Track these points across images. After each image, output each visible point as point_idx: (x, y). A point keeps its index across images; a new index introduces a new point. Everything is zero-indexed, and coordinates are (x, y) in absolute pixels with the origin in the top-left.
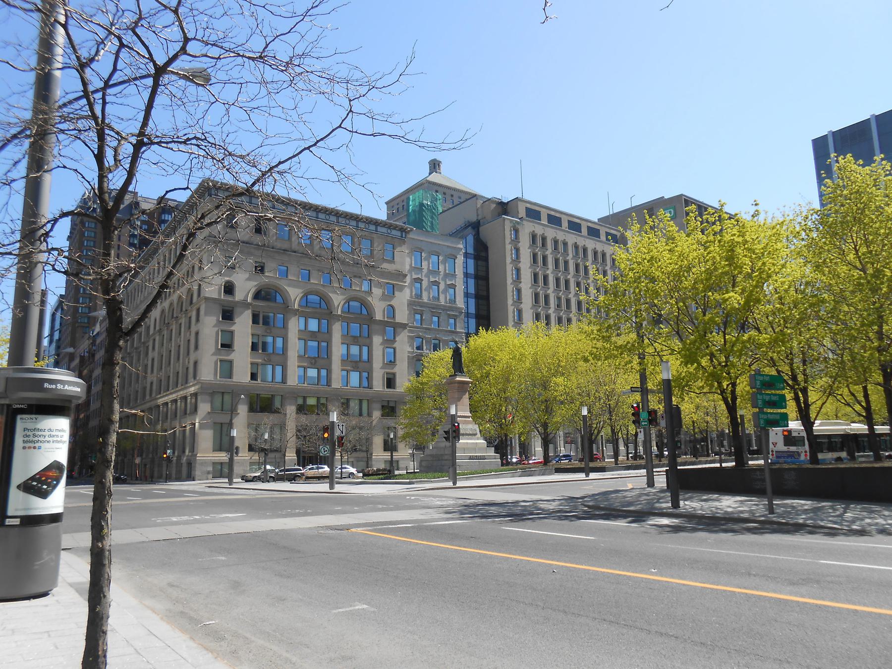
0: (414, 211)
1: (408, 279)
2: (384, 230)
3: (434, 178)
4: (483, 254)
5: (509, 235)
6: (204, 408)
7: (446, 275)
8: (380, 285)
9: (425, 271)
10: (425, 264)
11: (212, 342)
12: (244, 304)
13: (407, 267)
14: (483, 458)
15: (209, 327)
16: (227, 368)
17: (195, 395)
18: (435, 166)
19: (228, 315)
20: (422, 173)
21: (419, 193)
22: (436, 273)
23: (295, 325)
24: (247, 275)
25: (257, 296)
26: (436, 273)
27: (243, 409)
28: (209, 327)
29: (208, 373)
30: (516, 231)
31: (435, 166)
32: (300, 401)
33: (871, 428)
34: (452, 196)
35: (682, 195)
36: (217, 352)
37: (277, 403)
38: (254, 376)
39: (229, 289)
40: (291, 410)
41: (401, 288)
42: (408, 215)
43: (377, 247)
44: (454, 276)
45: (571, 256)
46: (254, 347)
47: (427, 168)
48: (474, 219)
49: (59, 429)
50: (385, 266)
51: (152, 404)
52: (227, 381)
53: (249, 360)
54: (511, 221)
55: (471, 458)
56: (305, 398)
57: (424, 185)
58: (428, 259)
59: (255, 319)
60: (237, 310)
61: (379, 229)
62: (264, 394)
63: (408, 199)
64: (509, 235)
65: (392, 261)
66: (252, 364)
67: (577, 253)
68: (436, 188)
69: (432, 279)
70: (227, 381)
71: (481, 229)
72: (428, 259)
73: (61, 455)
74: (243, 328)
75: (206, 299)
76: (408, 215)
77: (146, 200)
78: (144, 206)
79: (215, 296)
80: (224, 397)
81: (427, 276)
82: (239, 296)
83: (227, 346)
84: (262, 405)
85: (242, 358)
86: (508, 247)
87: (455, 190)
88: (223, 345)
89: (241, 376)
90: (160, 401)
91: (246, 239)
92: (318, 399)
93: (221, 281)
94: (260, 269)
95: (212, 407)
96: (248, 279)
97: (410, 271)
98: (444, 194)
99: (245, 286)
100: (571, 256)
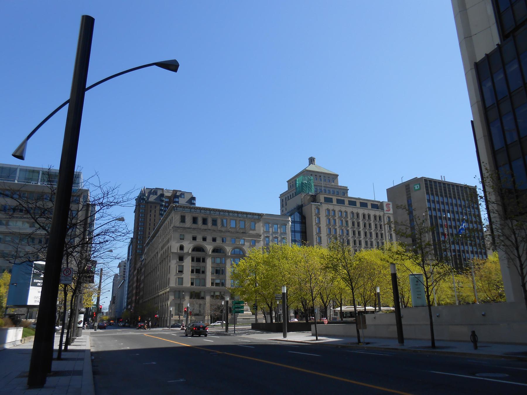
0: (299, 186)
1: (262, 237)
2: (250, 216)
3: (312, 168)
4: (304, 221)
5: (314, 211)
6: (171, 298)
7: (281, 234)
8: (249, 241)
9: (271, 232)
10: (271, 230)
11: (175, 271)
12: (188, 254)
13: (262, 231)
14: (249, 319)
15: (174, 264)
16: (181, 281)
17: (168, 292)
18: (312, 161)
19: (181, 259)
20: (304, 165)
21: (301, 177)
22: (276, 233)
23: (209, 262)
24: (189, 242)
25: (193, 250)
26: (276, 233)
27: (187, 298)
28: (174, 264)
29: (173, 283)
30: (318, 209)
31: (312, 161)
32: (212, 294)
33: (355, 308)
34: (320, 176)
35: (422, 177)
36: (177, 274)
37: (202, 295)
38: (192, 284)
39: (182, 248)
40: (208, 298)
41: (259, 242)
42: (296, 188)
43: (247, 225)
44: (285, 233)
45: (349, 218)
46: (192, 271)
47: (308, 162)
48: (300, 204)
49: (82, 315)
50: (251, 232)
51: (157, 295)
52: (180, 286)
53: (190, 277)
54: (315, 205)
55: (243, 319)
56: (214, 292)
57: (305, 173)
58: (272, 227)
59: (193, 260)
60: (185, 257)
61: (248, 216)
62: (197, 291)
63: (296, 181)
64: (314, 211)
65: (254, 230)
66: (191, 278)
67: (353, 216)
68: (311, 173)
69: (274, 236)
70: (180, 286)
71: (303, 208)
72: (272, 227)
73: (82, 319)
74: (188, 264)
75: (172, 253)
76: (296, 188)
77: (168, 191)
78: (166, 194)
79: (176, 251)
80: (179, 293)
81: (272, 235)
82: (185, 250)
83: (181, 272)
84: (196, 295)
85: (187, 277)
86: (314, 217)
87: (322, 173)
88: (179, 271)
89: (187, 284)
90: (160, 293)
91: (188, 226)
92: (220, 292)
93: (178, 245)
94: (194, 239)
95: (175, 298)
96: (190, 243)
97: (263, 233)
98: (316, 176)
99: (188, 246)
100: (349, 218)
